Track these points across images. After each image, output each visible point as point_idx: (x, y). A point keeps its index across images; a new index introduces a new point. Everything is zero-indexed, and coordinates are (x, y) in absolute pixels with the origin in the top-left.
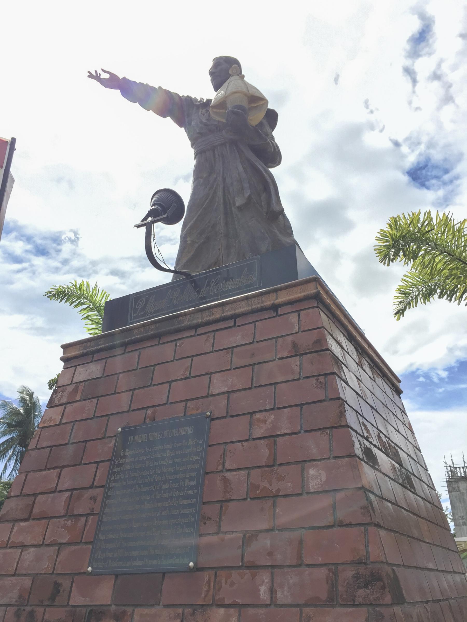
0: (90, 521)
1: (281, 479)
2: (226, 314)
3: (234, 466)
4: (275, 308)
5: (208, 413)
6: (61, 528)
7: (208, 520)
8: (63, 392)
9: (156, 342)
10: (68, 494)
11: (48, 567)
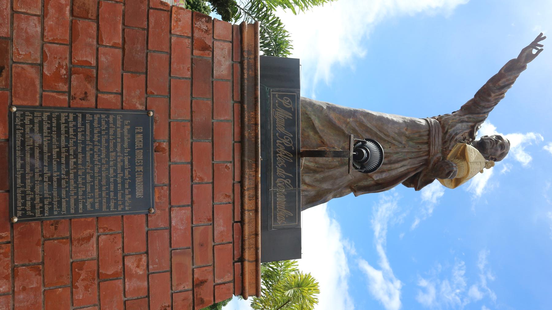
0: (61, 97)
1: (86, 288)
2: (246, 212)
3: (101, 244)
4: (242, 260)
5: (153, 211)
6: (59, 63)
7: (55, 227)
8: (207, 31)
9: (237, 138)
10: (93, 62)
11: (19, 54)
